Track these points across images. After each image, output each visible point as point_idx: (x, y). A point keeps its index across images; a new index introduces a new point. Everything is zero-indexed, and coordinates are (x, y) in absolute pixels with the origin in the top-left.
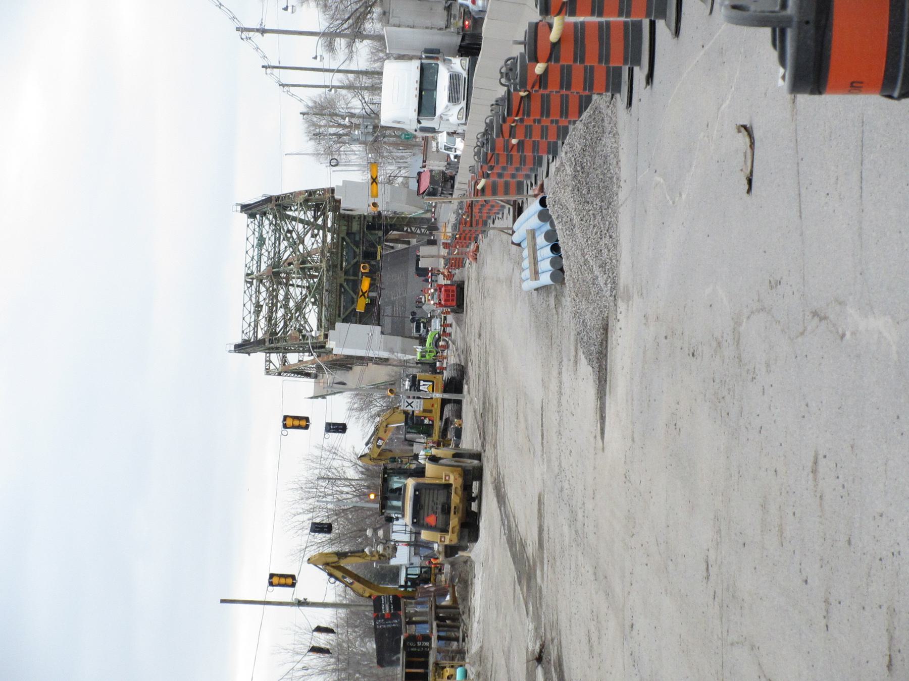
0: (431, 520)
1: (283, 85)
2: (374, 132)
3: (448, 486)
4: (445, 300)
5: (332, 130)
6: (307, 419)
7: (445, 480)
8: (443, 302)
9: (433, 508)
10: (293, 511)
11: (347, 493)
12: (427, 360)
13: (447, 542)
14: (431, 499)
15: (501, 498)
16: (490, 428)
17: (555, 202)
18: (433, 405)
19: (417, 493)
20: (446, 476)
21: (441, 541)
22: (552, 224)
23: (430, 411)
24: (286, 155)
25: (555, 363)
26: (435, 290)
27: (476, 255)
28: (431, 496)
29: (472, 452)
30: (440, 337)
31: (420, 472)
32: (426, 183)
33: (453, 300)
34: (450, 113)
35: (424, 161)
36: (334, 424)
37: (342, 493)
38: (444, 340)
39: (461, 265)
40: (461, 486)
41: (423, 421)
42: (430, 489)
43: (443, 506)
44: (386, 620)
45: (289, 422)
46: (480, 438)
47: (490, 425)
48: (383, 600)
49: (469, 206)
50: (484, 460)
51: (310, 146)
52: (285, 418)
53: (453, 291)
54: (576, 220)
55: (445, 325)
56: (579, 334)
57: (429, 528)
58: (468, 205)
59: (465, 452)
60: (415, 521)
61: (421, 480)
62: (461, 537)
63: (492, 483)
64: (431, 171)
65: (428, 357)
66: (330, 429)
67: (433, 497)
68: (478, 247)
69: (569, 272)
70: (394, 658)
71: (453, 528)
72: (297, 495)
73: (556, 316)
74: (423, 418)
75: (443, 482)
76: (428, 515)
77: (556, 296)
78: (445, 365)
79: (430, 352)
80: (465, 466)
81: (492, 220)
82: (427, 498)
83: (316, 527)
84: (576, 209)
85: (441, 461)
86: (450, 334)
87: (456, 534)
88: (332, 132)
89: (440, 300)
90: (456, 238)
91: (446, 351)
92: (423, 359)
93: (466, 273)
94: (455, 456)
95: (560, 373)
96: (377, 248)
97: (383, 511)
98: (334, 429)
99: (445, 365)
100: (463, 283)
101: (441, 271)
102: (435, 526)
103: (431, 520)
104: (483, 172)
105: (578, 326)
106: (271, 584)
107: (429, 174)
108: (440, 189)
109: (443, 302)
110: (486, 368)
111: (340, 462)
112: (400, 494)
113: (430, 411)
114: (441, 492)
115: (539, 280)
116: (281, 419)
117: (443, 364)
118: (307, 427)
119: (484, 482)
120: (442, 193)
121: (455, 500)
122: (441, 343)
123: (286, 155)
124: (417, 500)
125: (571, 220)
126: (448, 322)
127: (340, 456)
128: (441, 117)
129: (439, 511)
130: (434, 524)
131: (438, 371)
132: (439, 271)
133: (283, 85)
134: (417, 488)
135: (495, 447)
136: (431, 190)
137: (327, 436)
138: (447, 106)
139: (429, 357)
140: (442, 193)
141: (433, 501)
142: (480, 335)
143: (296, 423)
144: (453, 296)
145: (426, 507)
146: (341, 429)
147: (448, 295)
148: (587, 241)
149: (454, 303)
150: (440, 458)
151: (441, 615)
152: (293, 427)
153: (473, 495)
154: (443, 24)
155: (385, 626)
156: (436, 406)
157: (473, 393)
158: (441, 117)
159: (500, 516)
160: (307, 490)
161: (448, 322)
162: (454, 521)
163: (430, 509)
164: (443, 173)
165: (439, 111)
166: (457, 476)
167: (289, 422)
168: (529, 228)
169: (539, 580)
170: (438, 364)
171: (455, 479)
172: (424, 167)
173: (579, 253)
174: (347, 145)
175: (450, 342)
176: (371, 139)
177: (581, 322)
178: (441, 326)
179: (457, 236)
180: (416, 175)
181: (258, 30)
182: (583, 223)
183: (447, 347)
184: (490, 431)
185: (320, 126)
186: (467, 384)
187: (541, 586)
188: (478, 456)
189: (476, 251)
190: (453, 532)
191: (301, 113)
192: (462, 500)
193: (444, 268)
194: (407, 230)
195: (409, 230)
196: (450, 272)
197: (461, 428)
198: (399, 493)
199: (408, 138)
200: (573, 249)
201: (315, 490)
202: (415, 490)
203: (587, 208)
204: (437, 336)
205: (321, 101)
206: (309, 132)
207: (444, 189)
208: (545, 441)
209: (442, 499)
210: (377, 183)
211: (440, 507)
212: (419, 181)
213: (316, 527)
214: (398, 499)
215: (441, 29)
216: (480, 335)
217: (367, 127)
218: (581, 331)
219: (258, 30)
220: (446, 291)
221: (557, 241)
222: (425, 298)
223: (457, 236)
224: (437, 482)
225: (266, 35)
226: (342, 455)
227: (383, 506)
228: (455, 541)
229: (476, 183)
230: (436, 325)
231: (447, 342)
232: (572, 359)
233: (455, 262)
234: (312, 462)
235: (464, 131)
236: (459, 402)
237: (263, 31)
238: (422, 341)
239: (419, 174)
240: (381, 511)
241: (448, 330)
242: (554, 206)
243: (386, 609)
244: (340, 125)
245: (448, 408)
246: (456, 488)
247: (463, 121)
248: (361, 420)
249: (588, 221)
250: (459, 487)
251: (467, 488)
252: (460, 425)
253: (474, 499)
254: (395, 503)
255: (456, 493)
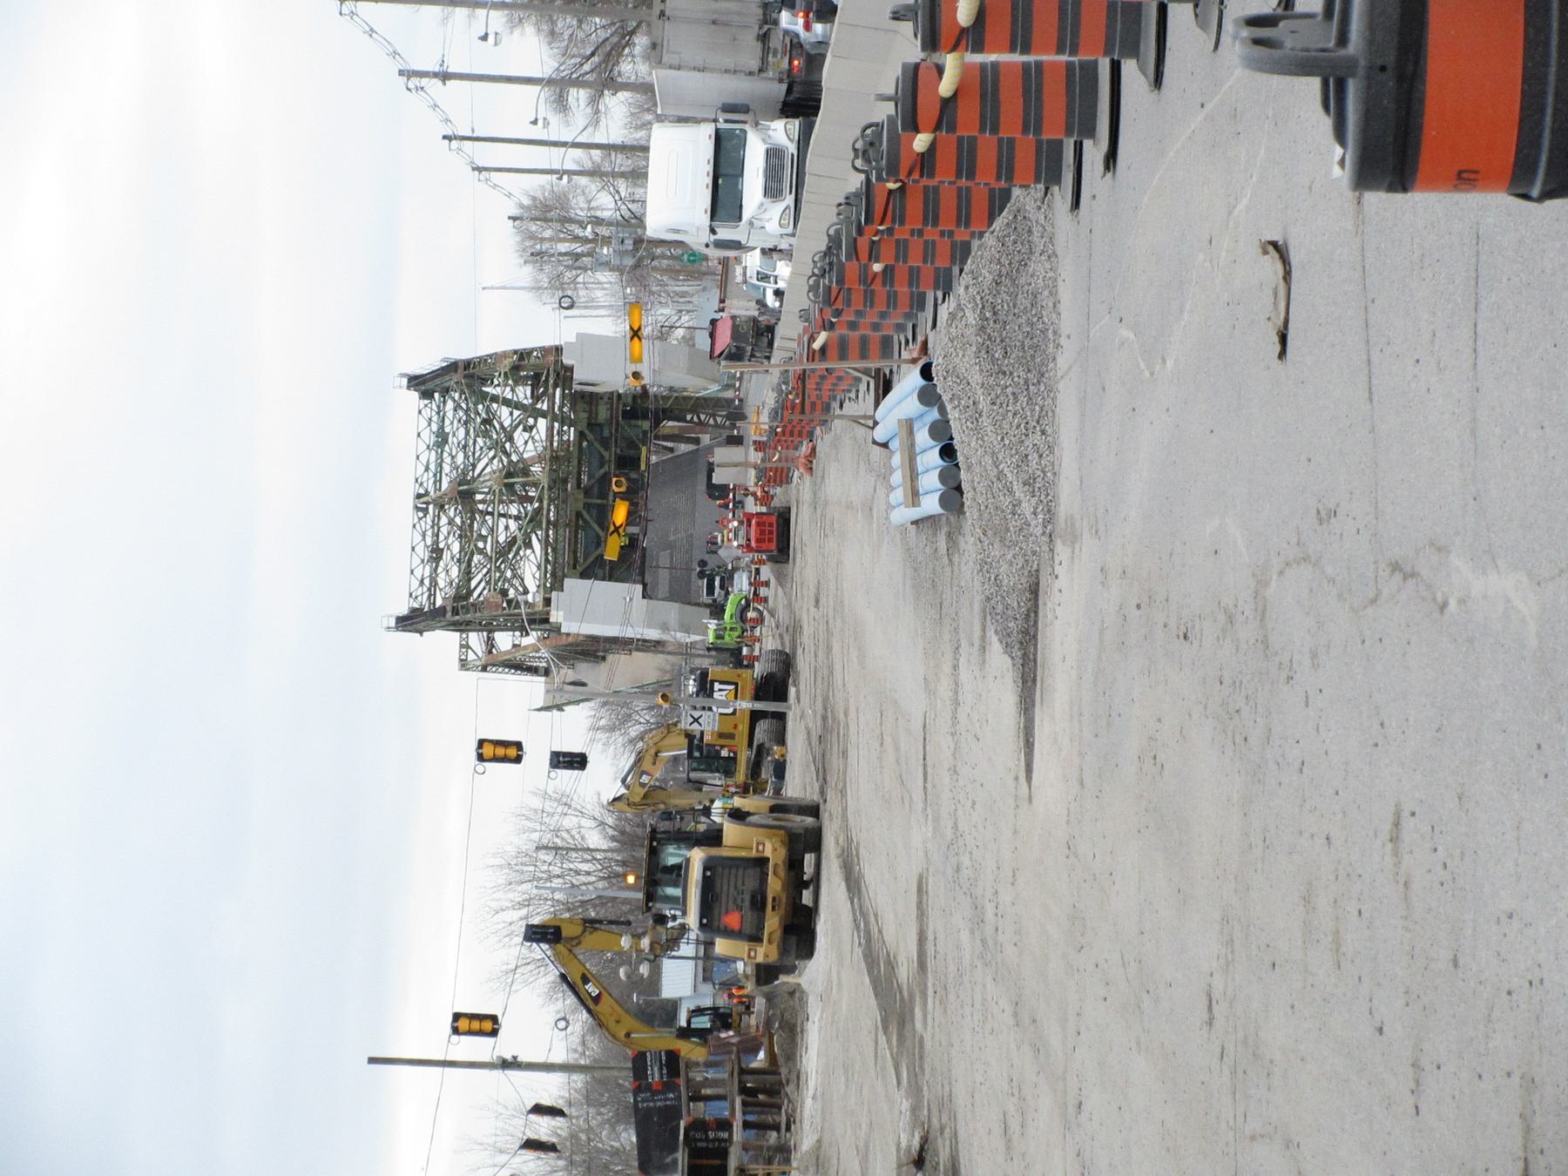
0: (733, 920)
1: (479, 169)
2: (636, 249)
3: (762, 862)
4: (758, 541)
5: (563, 247)
6: (519, 745)
7: (757, 850)
8: (753, 544)
9: (735, 899)
10: (494, 905)
11: (588, 873)
12: (727, 644)
13: (760, 959)
14: (732, 884)
15: (853, 883)
16: (835, 762)
17: (947, 372)
18: (736, 727)
19: (709, 873)
20: (758, 844)
21: (749, 956)
22: (942, 410)
23: (731, 736)
24: (484, 289)
25: (948, 649)
26: (741, 523)
27: (811, 462)
28: (733, 879)
29: (804, 803)
30: (748, 605)
31: (713, 837)
32: (724, 338)
33: (770, 540)
34: (766, 216)
35: (722, 301)
36: (565, 754)
37: (578, 873)
38: (755, 609)
39: (784, 480)
40: (784, 862)
41: (718, 752)
42: (730, 868)
43: (753, 897)
44: (654, 1093)
45: (488, 751)
46: (817, 780)
47: (835, 756)
48: (649, 1059)
49: (799, 378)
50: (825, 816)
51: (526, 274)
52: (481, 743)
53: (771, 525)
54: (984, 404)
55: (756, 584)
56: (988, 599)
57: (728, 933)
58: (797, 376)
59: (793, 803)
60: (705, 921)
61: (715, 852)
62: (784, 951)
63: (838, 857)
64: (733, 318)
65: (727, 639)
66: (559, 762)
67: (736, 881)
68: (814, 449)
69: (972, 492)
70: (669, 1160)
71: (770, 934)
72: (502, 877)
73: (948, 569)
74: (718, 748)
75: (754, 854)
76: (727, 912)
77: (949, 535)
78: (756, 653)
79: (732, 629)
80: (791, 828)
81: (838, 403)
82: (725, 882)
83: (534, 933)
84: (983, 384)
85: (751, 819)
86: (766, 600)
87: (775, 946)
88: (563, 251)
89: (749, 540)
90: (776, 434)
91: (758, 629)
92: (719, 641)
93: (794, 492)
94: (773, 809)
95: (955, 667)
96: (640, 449)
97: (650, 904)
98: (564, 762)
99: (756, 653)
100: (789, 509)
101: (751, 489)
102: (740, 931)
103: (733, 920)
104: (823, 320)
105: (986, 586)
106: (456, 1031)
107: (730, 323)
108: (749, 348)
109: (753, 544)
110: (828, 659)
111: (575, 820)
112: (679, 875)
113: (731, 736)
114: (750, 871)
115: (919, 506)
116: (475, 745)
117: (753, 650)
118: (518, 760)
119: (824, 855)
120: (752, 356)
121: (775, 885)
122: (751, 614)
123: (484, 289)
124: (708, 885)
125: (974, 403)
126: (763, 578)
127: (576, 809)
128: (751, 224)
129: (747, 903)
130: (737, 927)
131: (745, 663)
132: (747, 490)
133: (479, 169)
134: (708, 866)
135: (843, 793)
136: (734, 350)
137: (553, 775)
138: (762, 204)
139: (730, 639)
140: (752, 356)
141: (736, 888)
142: (817, 601)
143: (500, 751)
144: (771, 532)
145: (724, 900)
146: (577, 762)
147: (763, 532)
148: (1003, 439)
149: (773, 546)
150: (748, 814)
151: (749, 1085)
152: (495, 759)
153: (805, 878)
154: (754, 64)
155: (651, 1104)
156: (740, 727)
157: (805, 699)
158: (751, 224)
159: (851, 915)
160: (517, 868)
161: (763, 578)
162: (772, 922)
163: (731, 903)
164: (755, 320)
165: (746, 215)
166: (778, 845)
167: (488, 751)
168: (903, 417)
169: (919, 1025)
170: (745, 651)
171: (775, 850)
172: (722, 310)
173: (988, 460)
174: (589, 272)
175: (765, 613)
176: (629, 262)
177: (993, 578)
178: (750, 584)
179: (779, 430)
180: (707, 324)
181: (436, 75)
182: (995, 408)
183: (760, 620)
184: (835, 766)
185: (542, 240)
186: (795, 686)
187: (922, 1037)
188: (814, 810)
189: (810, 455)
190: (770, 942)
191: (510, 218)
192: (786, 887)
193: (756, 484)
194: (692, 418)
195: (695, 419)
196: (767, 493)
197: (785, 761)
198: (677, 873)
199: (694, 261)
200: (979, 453)
201: (532, 868)
202: (705, 869)
203: (1002, 382)
204: (743, 602)
205: (544, 197)
206: (524, 250)
207: (756, 348)
208: (929, 786)
209: (751, 884)
210: (640, 339)
211: (747, 898)
212: (712, 335)
213: (534, 933)
214: (676, 885)
215: (751, 73)
216: (817, 601)
217: (622, 242)
218: (992, 594)
219: (436, 75)
220: (758, 524)
221: (952, 439)
222: (723, 536)
223: (779, 430)
224: (743, 854)
225: (451, 83)
226: (579, 807)
227: (650, 897)
228: (774, 957)
229: (812, 339)
230: (742, 583)
231: (761, 613)
232: (977, 642)
233: (775, 474)
234: (528, 819)
235: (791, 245)
236: (781, 717)
237: (445, 76)
238: (717, 610)
239: (713, 322)
240: (647, 904)
241: (763, 591)
242: (945, 379)
243: (655, 1075)
244: (576, 238)
245: (762, 727)
246: (776, 865)
247: (790, 230)
248: (612, 747)
249: (1004, 405)
250: (780, 863)
251: (794, 864)
252: (783, 756)
253: (806, 885)
254: (671, 891)
255: (775, 873)
